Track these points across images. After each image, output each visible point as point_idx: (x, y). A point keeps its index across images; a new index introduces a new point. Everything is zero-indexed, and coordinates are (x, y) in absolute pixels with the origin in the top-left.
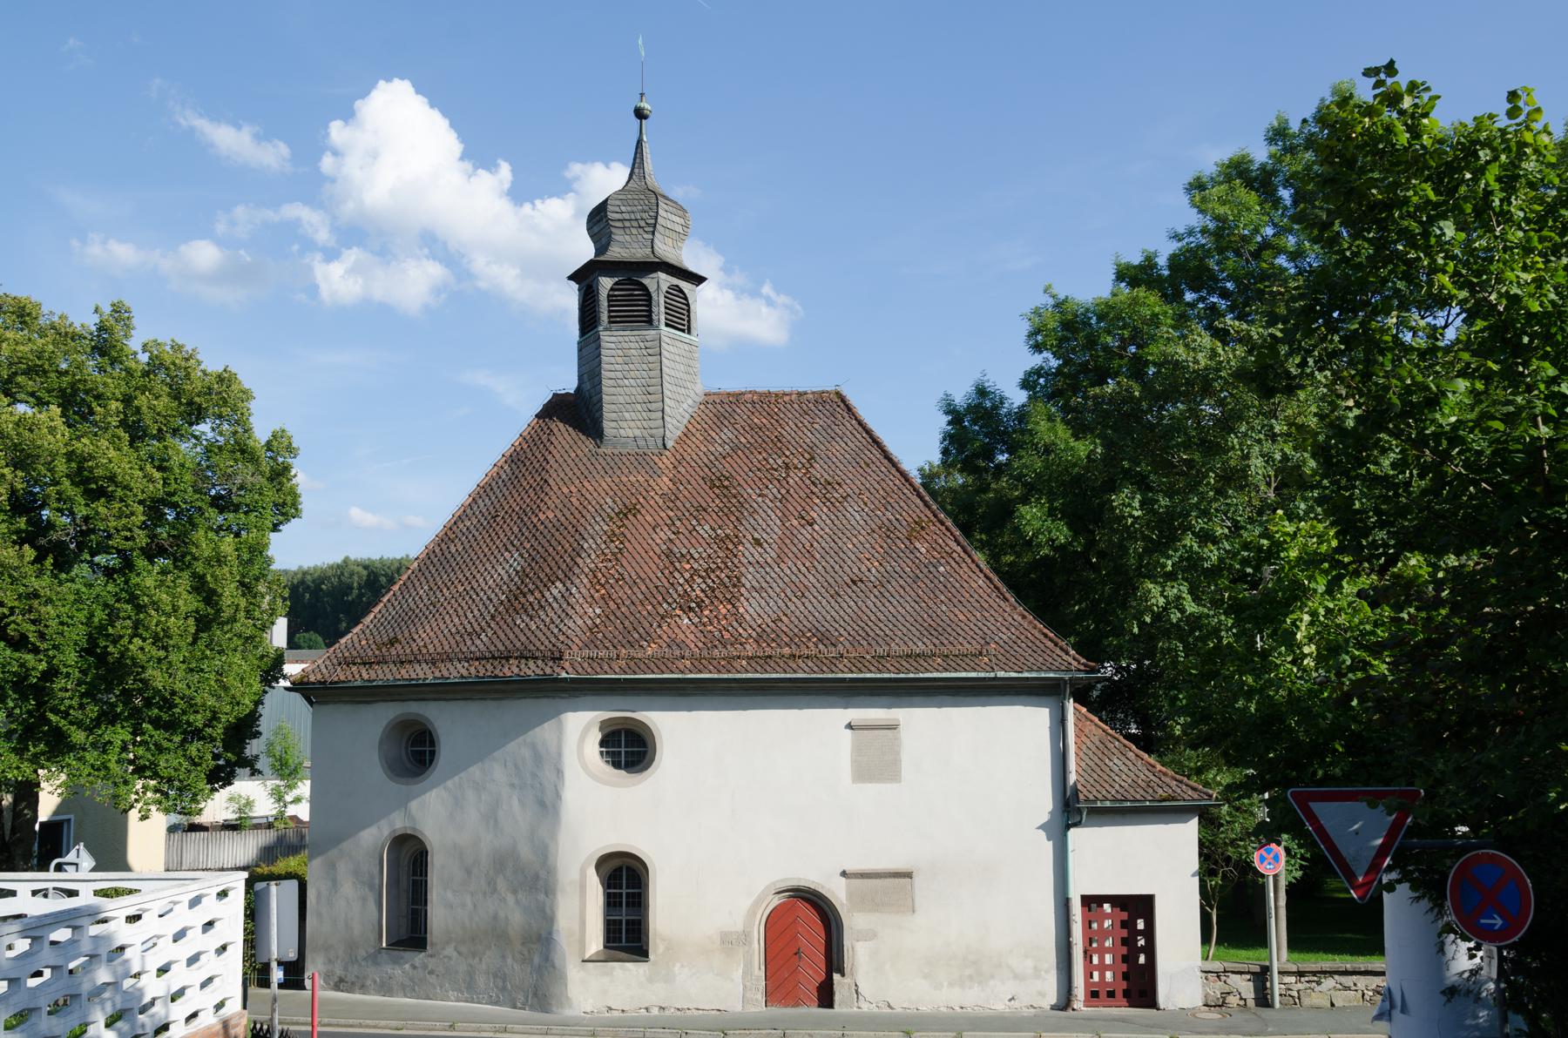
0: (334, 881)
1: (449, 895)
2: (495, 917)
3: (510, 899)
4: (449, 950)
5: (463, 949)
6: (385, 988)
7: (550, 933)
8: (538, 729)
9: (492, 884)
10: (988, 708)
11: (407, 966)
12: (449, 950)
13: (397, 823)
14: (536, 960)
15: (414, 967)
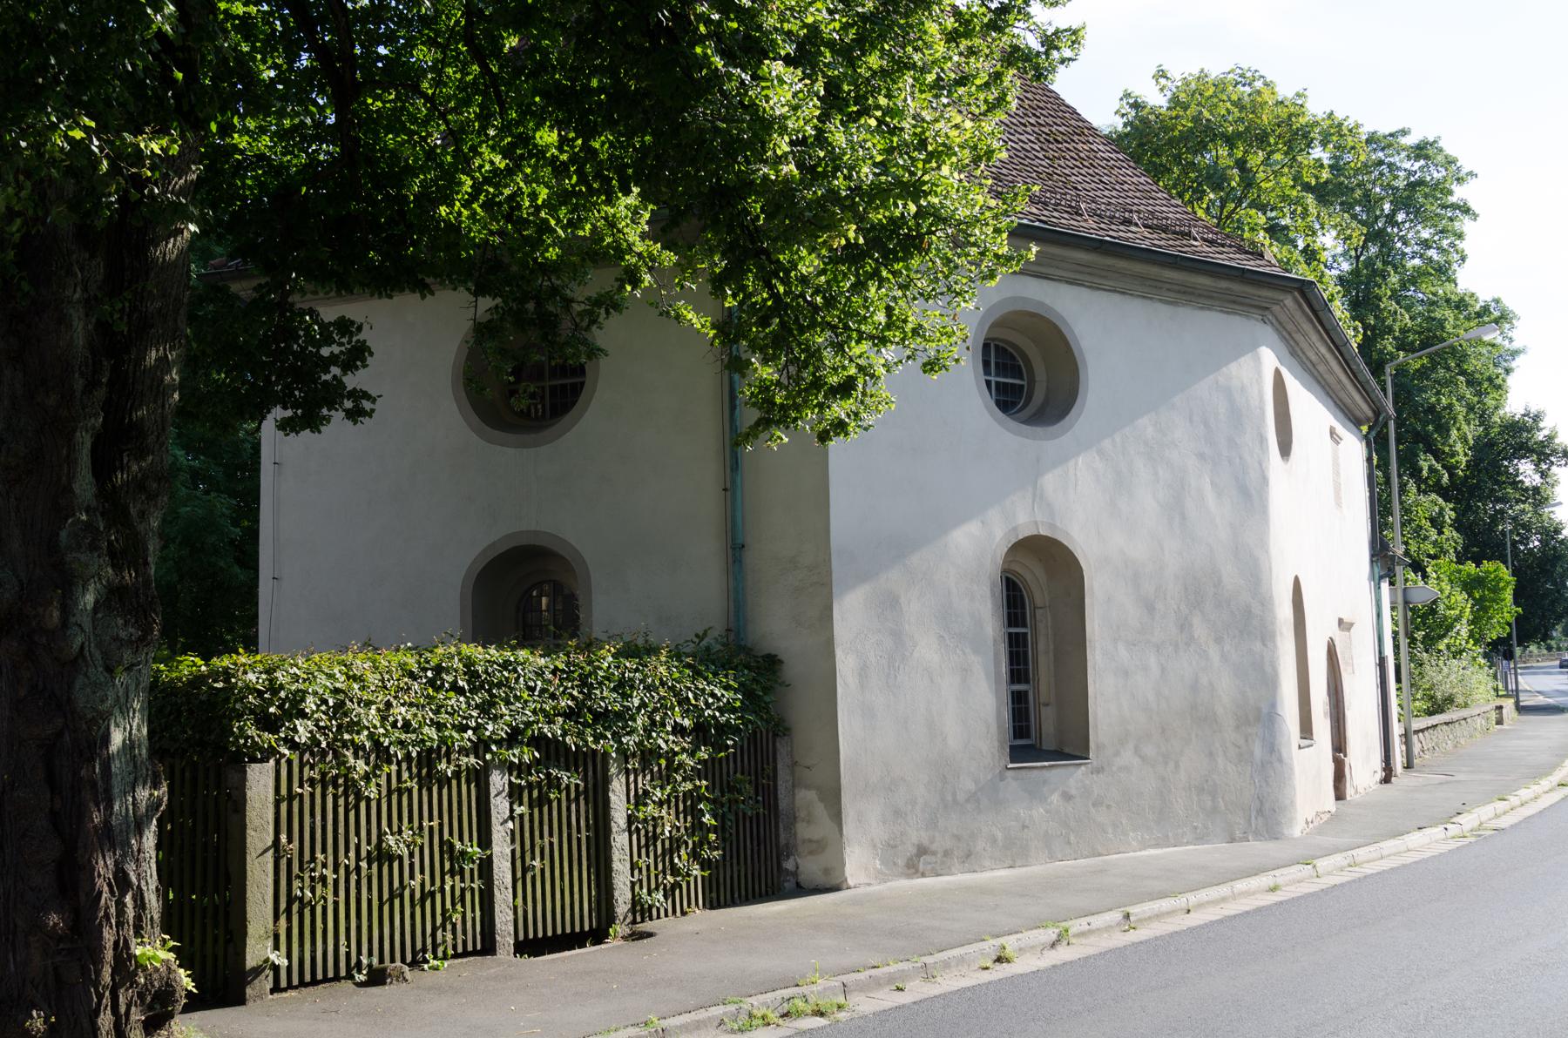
0: (898, 636)
1: (1123, 652)
2: (1195, 687)
3: (1214, 653)
4: (1127, 757)
5: (1149, 750)
6: (1014, 851)
7: (1273, 705)
8: (1233, 367)
9: (1184, 626)
10: (1320, 405)
11: (1055, 798)
12: (1127, 757)
13: (1021, 517)
14: (1258, 751)
15: (1067, 797)
